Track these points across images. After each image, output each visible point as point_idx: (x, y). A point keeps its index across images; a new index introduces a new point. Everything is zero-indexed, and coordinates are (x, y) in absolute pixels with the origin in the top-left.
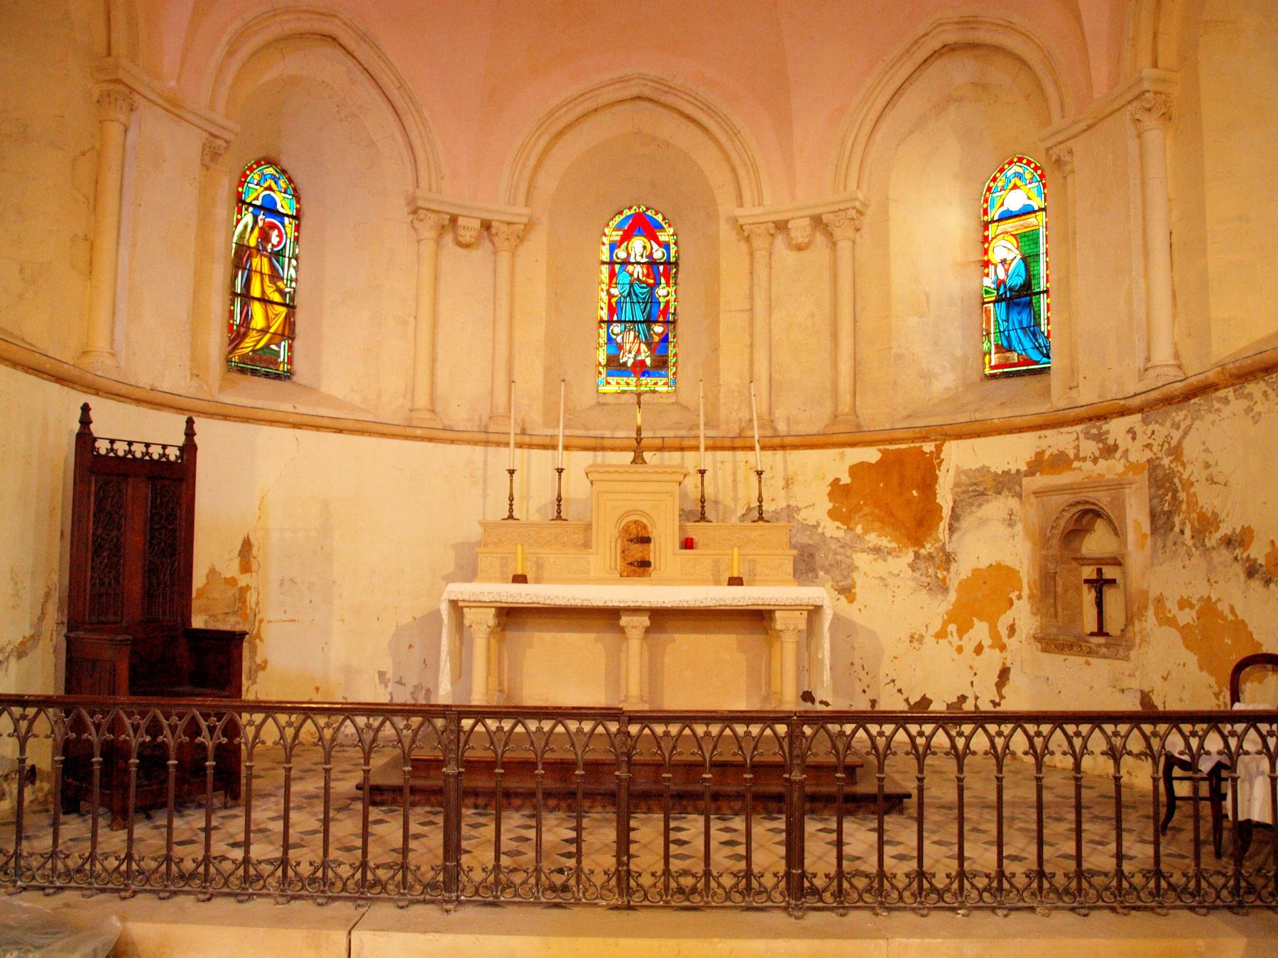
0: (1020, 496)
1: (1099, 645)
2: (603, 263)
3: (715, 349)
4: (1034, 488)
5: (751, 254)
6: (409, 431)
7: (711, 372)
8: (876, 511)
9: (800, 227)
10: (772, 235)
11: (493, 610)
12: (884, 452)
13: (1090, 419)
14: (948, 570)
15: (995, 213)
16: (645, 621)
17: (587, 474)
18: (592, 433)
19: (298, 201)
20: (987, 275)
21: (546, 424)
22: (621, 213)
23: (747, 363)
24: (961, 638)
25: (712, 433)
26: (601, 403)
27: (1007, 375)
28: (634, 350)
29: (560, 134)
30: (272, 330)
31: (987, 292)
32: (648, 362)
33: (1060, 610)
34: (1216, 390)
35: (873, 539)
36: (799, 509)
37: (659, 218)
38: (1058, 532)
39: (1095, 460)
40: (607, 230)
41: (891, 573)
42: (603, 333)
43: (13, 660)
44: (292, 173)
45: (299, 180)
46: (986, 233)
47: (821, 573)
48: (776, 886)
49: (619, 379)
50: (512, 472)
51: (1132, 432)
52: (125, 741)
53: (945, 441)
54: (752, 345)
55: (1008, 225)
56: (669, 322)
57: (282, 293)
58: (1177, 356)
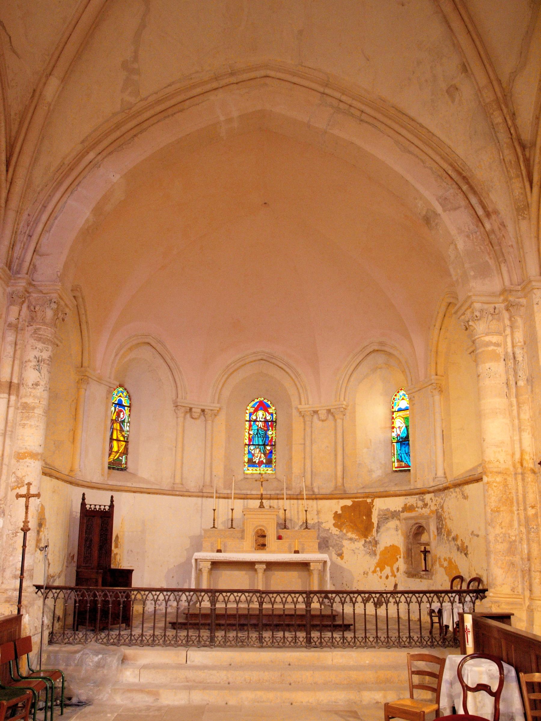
0: (400, 520)
1: (423, 575)
2: (247, 421)
3: (291, 459)
4: (404, 517)
5: (305, 422)
6: (174, 493)
7: (290, 467)
8: (351, 524)
9: (323, 414)
10: (313, 416)
11: (210, 562)
12: (354, 502)
13: (420, 494)
14: (376, 547)
15: (396, 408)
16: (264, 566)
17: (243, 512)
18: (244, 492)
19: (130, 401)
20: (393, 432)
21: (225, 488)
22: (254, 400)
23: (303, 465)
24: (381, 573)
25: (289, 492)
26: (246, 478)
27: (401, 471)
28: (259, 456)
29: (231, 374)
30: (120, 452)
31: (394, 439)
32: (264, 461)
33: (413, 561)
34: (450, 489)
35: (350, 535)
36: (322, 523)
37: (269, 403)
38: (412, 534)
39: (422, 509)
40: (248, 408)
41: (356, 548)
42: (246, 449)
43: (57, 579)
44: (128, 389)
45: (131, 392)
46: (393, 416)
47: (331, 548)
48: (303, 641)
49: (253, 468)
50: (214, 510)
51: (431, 499)
52: (119, 600)
53: (374, 498)
54: (305, 457)
55: (401, 413)
56: (272, 445)
57: (124, 437)
58: (445, 474)
